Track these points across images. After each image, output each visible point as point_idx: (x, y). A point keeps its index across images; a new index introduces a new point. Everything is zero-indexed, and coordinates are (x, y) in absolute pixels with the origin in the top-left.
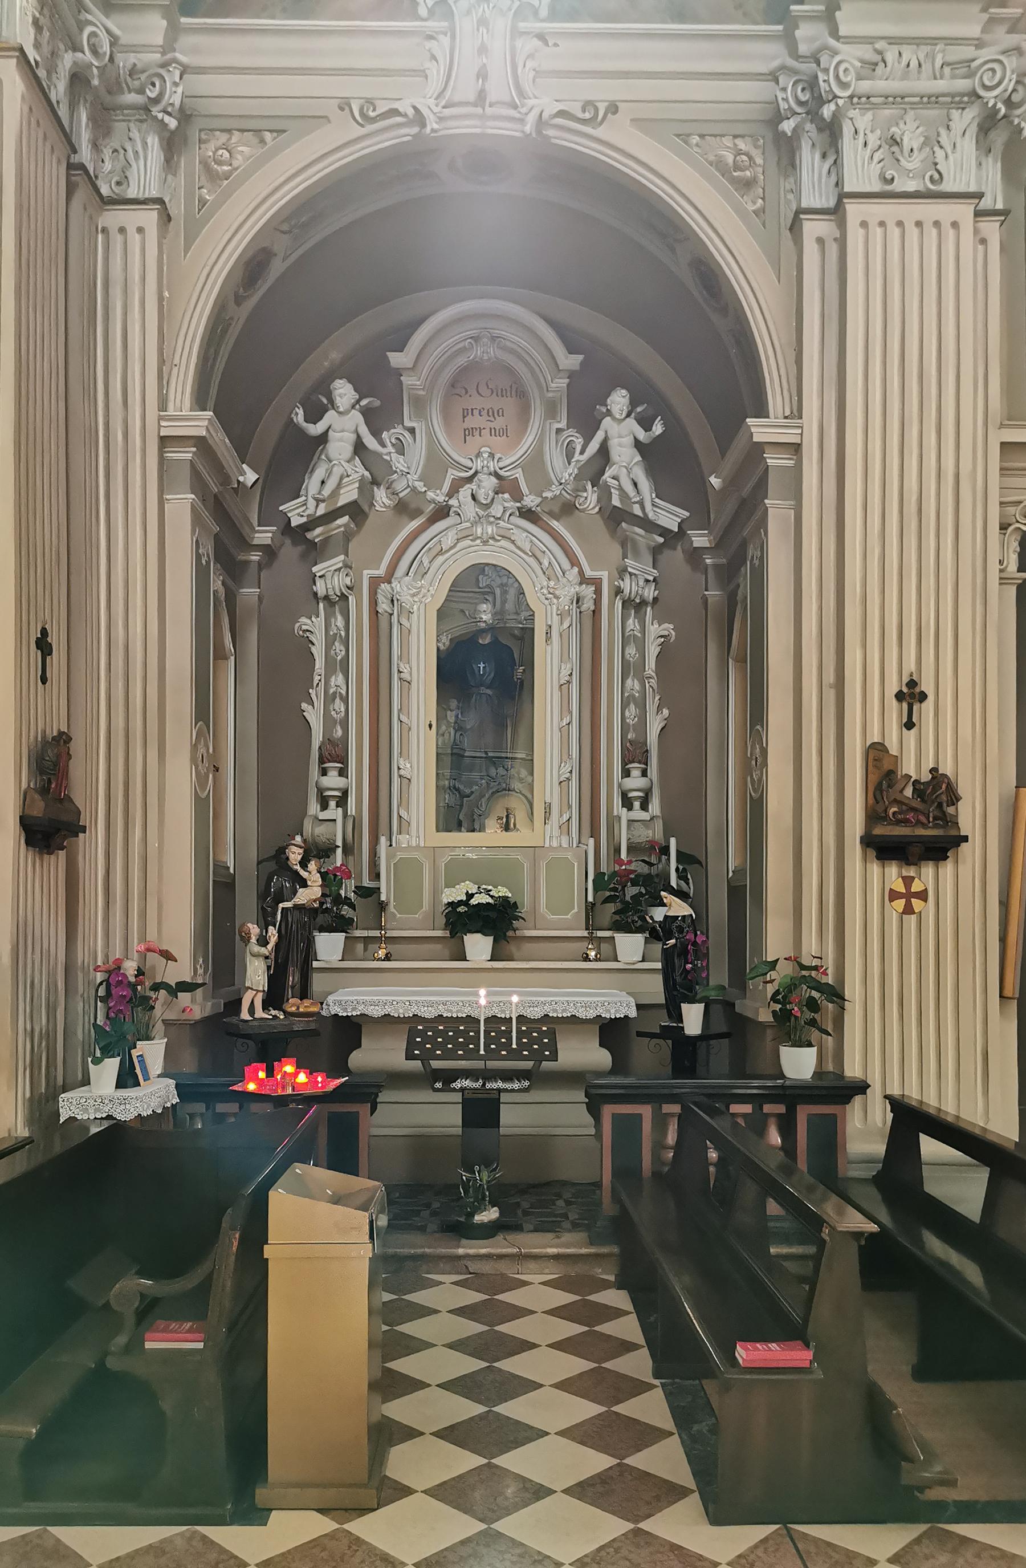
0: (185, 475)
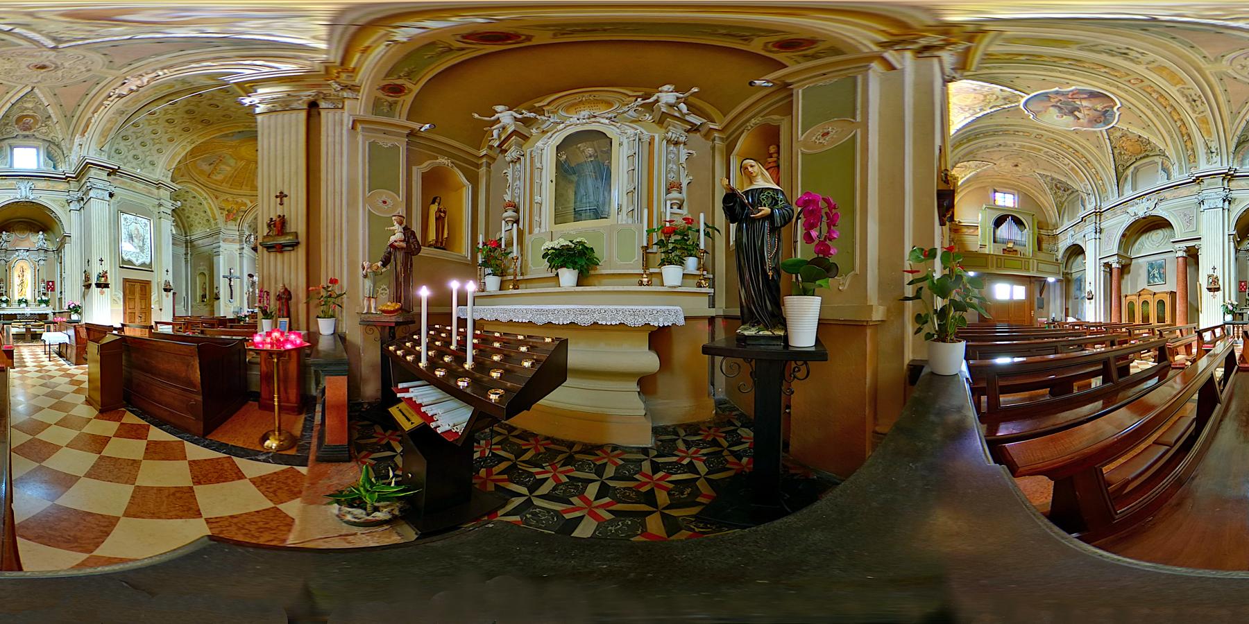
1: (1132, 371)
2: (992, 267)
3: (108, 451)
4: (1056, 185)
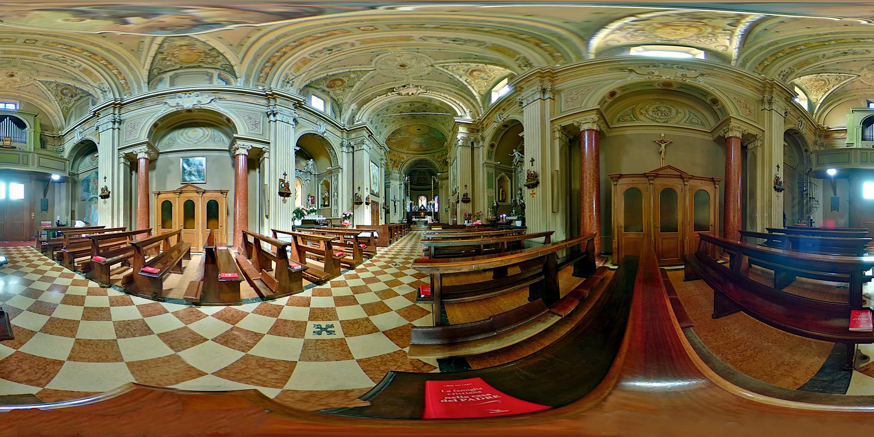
1: (527, 293)
2: (856, 161)
4: (62, 92)
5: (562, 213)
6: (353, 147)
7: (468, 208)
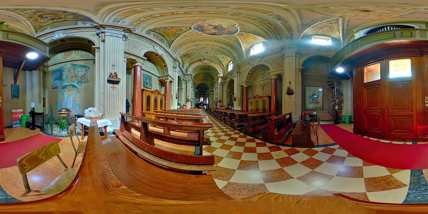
0: (301, 71)
3: (237, 141)
5: (241, 106)
6: (186, 81)
7: (221, 104)
